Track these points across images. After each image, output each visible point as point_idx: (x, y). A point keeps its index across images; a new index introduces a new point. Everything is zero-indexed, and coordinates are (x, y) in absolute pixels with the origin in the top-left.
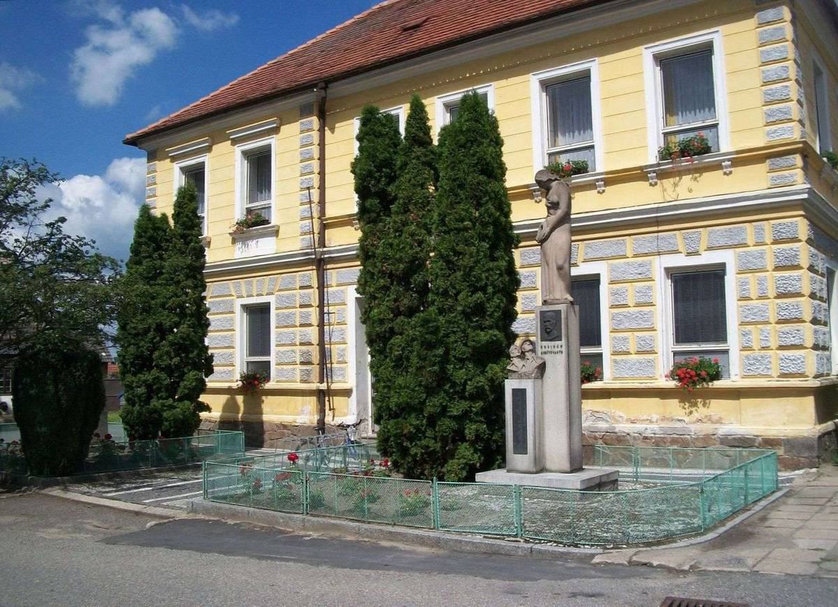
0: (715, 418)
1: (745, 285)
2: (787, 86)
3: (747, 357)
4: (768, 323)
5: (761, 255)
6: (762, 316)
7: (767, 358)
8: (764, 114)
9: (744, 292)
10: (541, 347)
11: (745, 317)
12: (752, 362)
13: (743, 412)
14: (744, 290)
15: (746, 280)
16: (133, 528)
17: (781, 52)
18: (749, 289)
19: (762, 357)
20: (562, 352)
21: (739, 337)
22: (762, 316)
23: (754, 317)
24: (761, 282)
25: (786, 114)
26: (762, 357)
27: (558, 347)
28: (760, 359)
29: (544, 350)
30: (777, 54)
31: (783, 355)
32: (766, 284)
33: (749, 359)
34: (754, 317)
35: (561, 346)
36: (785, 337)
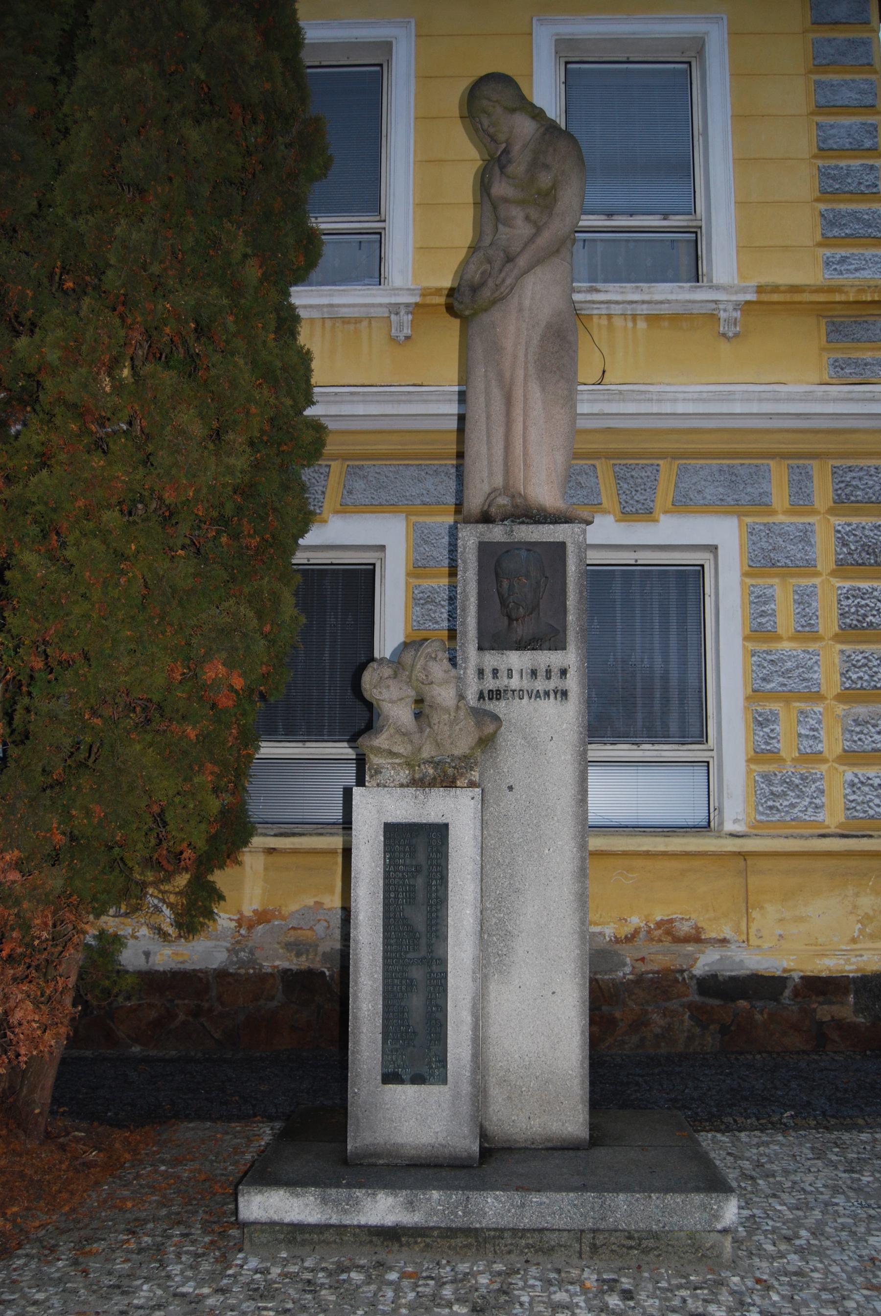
0: (684, 928)
1: (765, 603)
2: (872, 167)
3: (767, 778)
4: (818, 697)
5: (805, 536)
6: (804, 680)
7: (814, 782)
8: (819, 219)
9: (764, 620)
10: (481, 673)
11: (764, 679)
12: (780, 789)
13: (755, 914)
14: (763, 614)
15: (768, 592)
16: (690, 948)
17: (862, 92)
18: (773, 614)
19: (803, 778)
20: (565, 694)
21: (747, 727)
22: (804, 680)
23: (785, 681)
24: (804, 598)
25: (870, 226)
26: (803, 778)
27: (510, 676)
28: (797, 781)
29: (490, 684)
30: (854, 96)
31: (856, 775)
32: (814, 604)
33: (770, 783)
34: (785, 681)
35: (564, 672)
36: (861, 732)
